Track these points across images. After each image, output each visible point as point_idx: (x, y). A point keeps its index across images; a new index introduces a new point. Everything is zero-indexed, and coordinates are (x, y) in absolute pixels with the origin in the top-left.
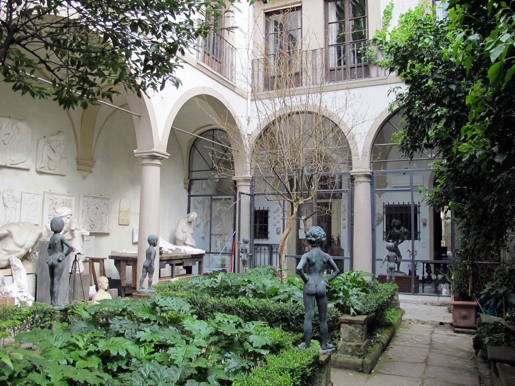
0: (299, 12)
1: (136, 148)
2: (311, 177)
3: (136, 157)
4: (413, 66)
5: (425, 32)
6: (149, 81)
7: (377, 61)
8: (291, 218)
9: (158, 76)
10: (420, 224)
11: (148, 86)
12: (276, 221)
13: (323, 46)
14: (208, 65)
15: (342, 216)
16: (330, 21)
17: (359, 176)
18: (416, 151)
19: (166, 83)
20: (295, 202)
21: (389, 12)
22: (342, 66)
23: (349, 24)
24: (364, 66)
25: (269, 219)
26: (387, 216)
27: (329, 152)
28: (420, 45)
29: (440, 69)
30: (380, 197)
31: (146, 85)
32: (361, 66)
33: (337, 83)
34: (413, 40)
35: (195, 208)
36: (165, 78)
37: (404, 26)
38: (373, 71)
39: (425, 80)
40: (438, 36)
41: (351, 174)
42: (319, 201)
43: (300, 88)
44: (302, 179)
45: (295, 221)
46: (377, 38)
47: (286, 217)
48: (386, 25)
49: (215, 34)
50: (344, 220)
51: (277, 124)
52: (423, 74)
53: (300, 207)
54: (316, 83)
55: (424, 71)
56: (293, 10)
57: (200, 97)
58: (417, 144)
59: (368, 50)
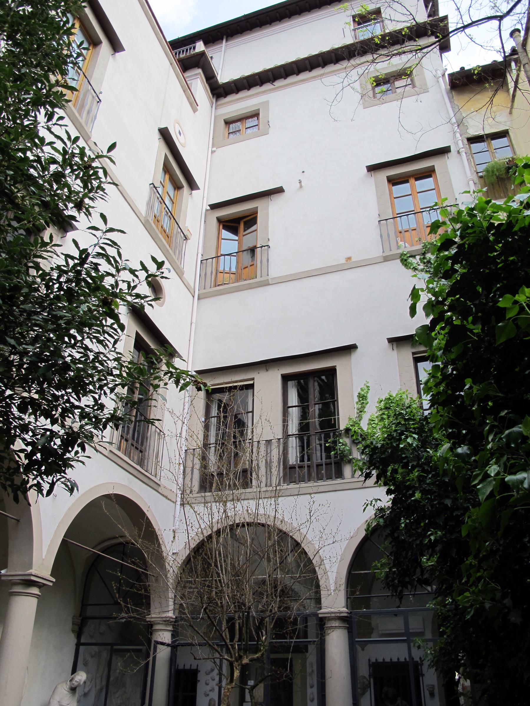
0: (250, 391)
1: (5, 567)
2: (263, 619)
3: (3, 580)
4: (395, 471)
5: (407, 430)
6: (33, 479)
7: (351, 457)
8: (229, 687)
9: (48, 473)
10: (425, 693)
11: (31, 487)
12: (208, 688)
13: (280, 436)
14: (125, 455)
15: (309, 681)
16: (290, 405)
17: (330, 619)
18: (407, 588)
19: (56, 486)
20: (237, 661)
21: (364, 396)
22: (306, 463)
23: (315, 409)
24: (335, 463)
25: (199, 685)
26: (375, 679)
27: (289, 582)
28: (401, 446)
29: (430, 478)
30: (363, 650)
31: (28, 486)
32: (331, 464)
33: (297, 486)
34: (393, 438)
35: (86, 664)
36: (55, 480)
37: (383, 414)
38: (347, 470)
39: (411, 492)
40: (423, 435)
41: (320, 616)
42: (273, 656)
43: (248, 490)
44: (247, 625)
45: (238, 690)
46: (351, 428)
47: (224, 683)
48: (361, 411)
49: (139, 413)
50: (312, 687)
51: (214, 540)
52: (408, 483)
53: (244, 669)
54: (271, 486)
55: (409, 480)
56: (242, 388)
57: (107, 497)
58: (407, 579)
59: (340, 443)
